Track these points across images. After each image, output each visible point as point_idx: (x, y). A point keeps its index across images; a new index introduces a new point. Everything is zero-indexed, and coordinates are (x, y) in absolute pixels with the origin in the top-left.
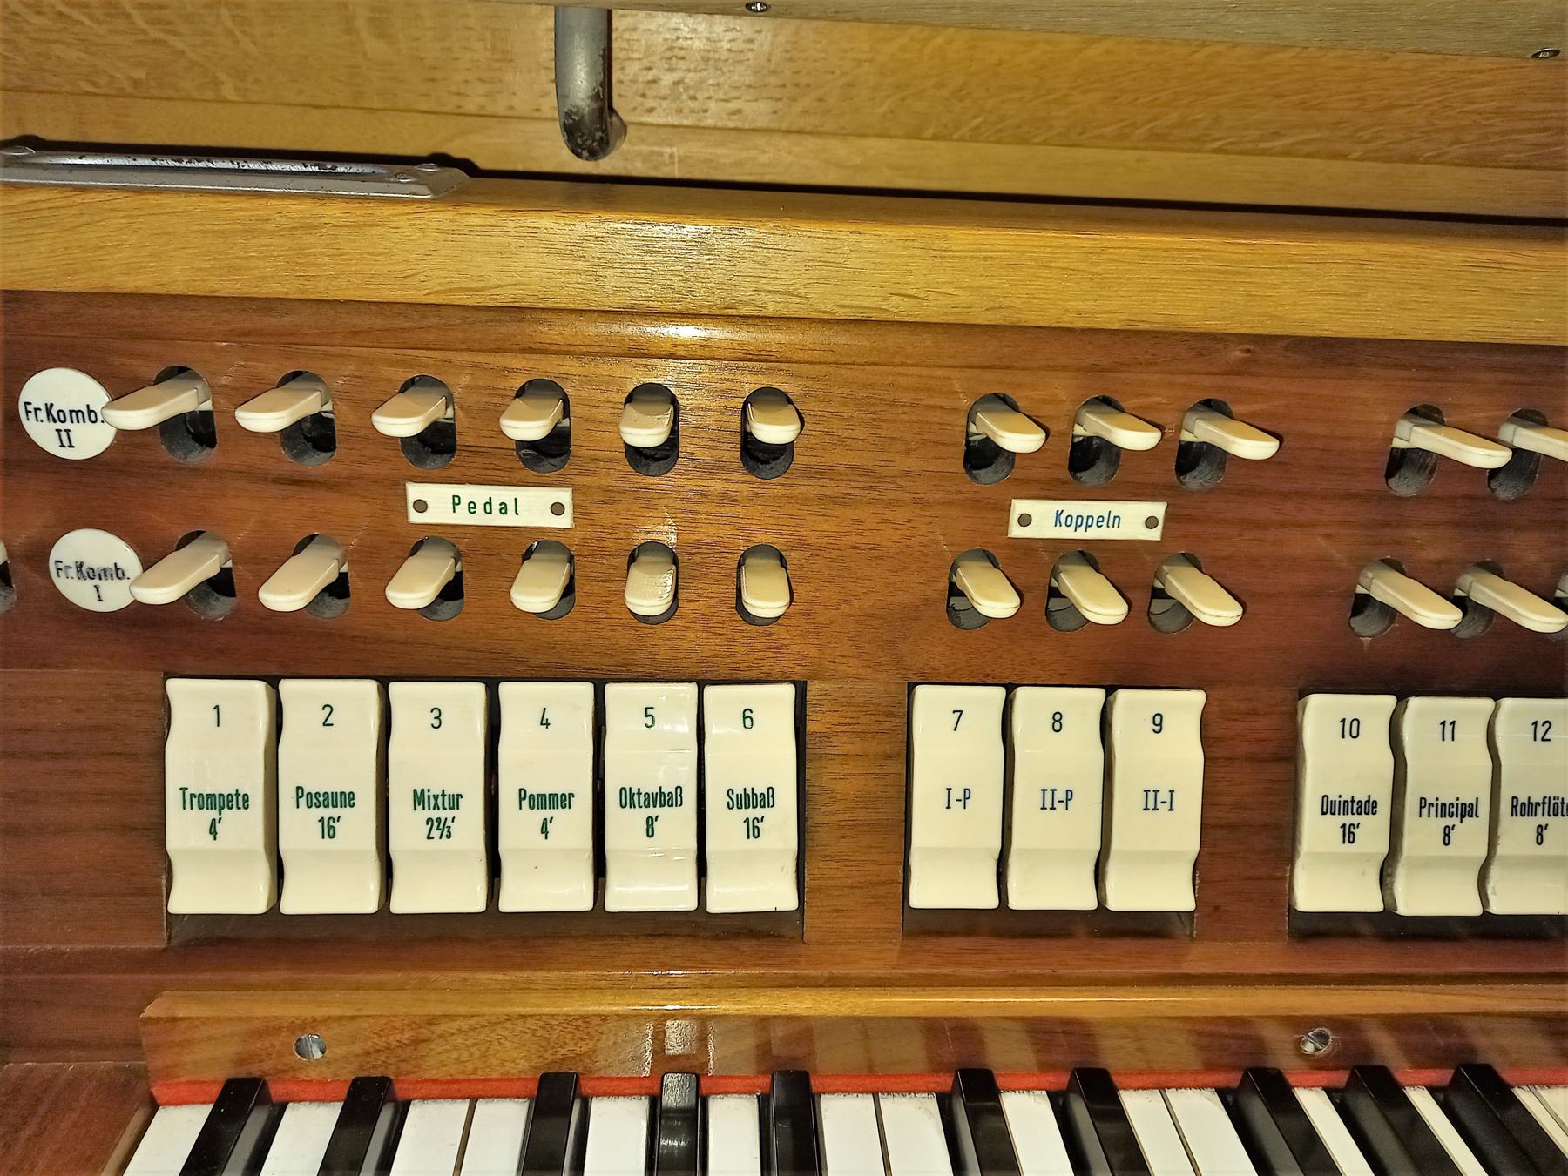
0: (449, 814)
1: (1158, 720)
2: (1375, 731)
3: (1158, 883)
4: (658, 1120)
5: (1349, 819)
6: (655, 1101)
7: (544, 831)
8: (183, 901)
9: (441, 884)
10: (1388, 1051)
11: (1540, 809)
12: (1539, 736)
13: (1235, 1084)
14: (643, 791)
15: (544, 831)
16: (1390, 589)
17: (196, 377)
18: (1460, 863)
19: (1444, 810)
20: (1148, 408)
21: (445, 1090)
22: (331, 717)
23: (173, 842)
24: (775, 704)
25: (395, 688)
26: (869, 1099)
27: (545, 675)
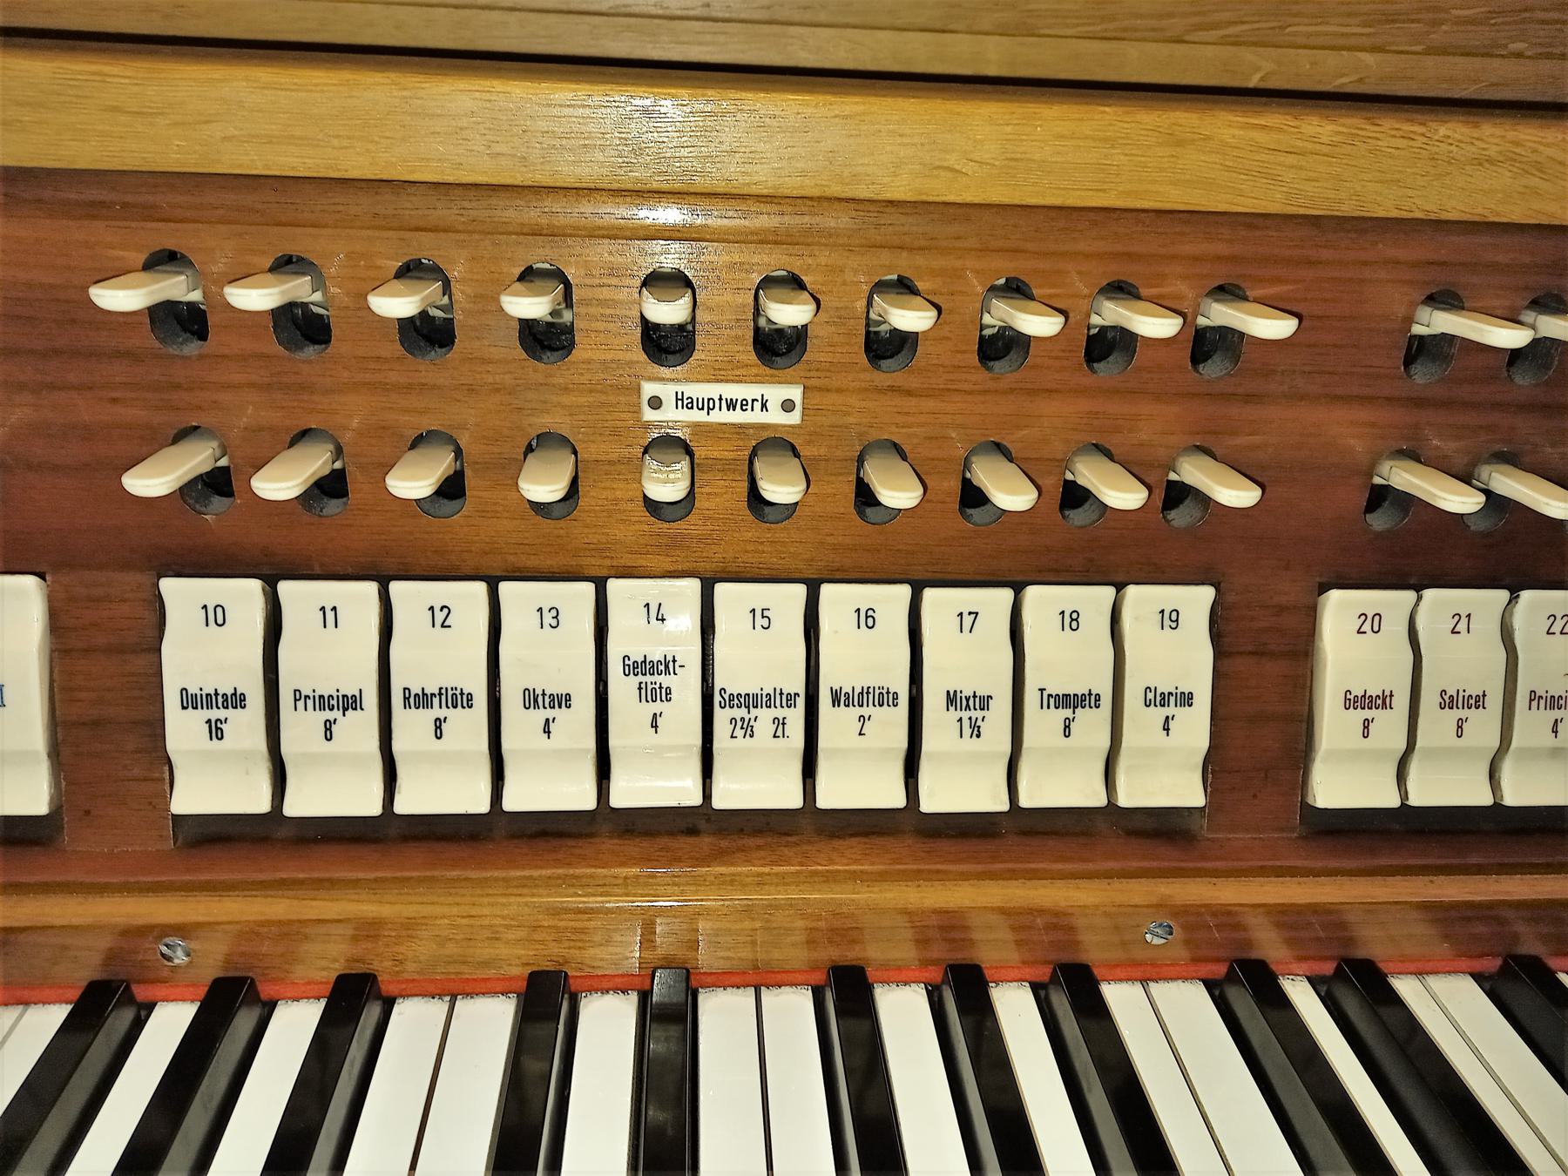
0: (979, 714)
2: (1396, 628)
3: (1166, 775)
4: (650, 1016)
5: (215, 714)
6: (645, 997)
7: (547, 731)
8: (184, 801)
10: (1270, 946)
11: (436, 701)
12: (439, 621)
13: (1046, 979)
14: (221, 692)
15: (547, 731)
16: (1405, 477)
18: (1378, 755)
19: (323, 703)
20: (1162, 296)
21: (727, 979)
24: (1197, 601)
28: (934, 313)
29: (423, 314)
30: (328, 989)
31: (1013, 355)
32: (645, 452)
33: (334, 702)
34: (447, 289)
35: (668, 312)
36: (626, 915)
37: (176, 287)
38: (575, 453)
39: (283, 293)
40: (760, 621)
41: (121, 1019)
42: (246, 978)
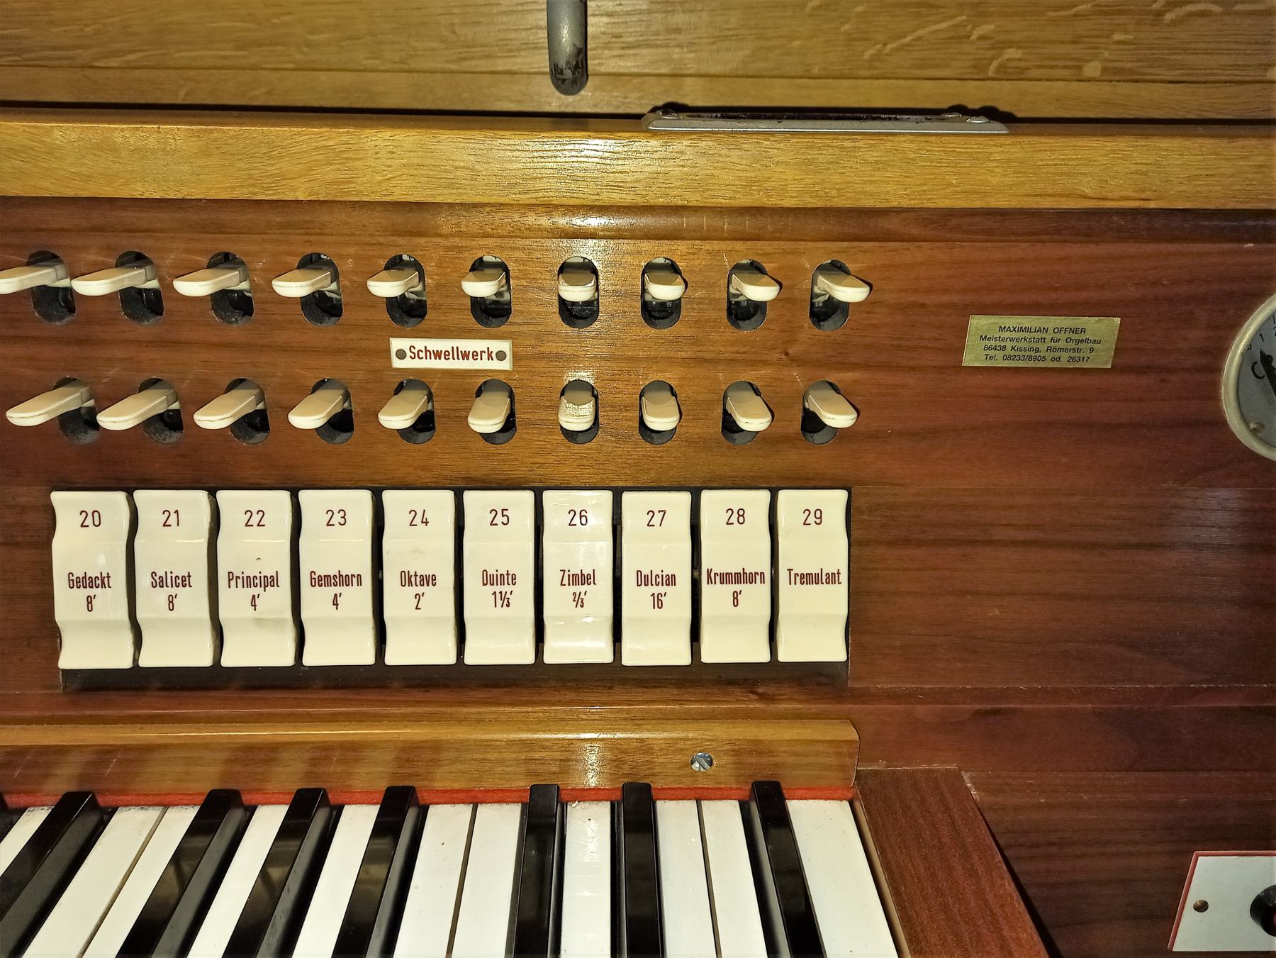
1: (818, 514)
8: (67, 661)
9: (340, 643)
17: (61, 262)
19: (249, 582)
21: (451, 797)
22: (173, 520)
23: (61, 616)
24: (834, 502)
25: (304, 495)
26: (693, 804)
27: (577, 484)
28: (777, 288)
29: (403, 296)
30: (202, 798)
31: (836, 317)
32: (562, 394)
33: (257, 581)
34: (422, 278)
35: (577, 293)
36: (590, 745)
37: (230, 280)
38: (596, 397)
39: (313, 284)
40: (499, 519)
41: (236, 816)
42: (317, 791)
